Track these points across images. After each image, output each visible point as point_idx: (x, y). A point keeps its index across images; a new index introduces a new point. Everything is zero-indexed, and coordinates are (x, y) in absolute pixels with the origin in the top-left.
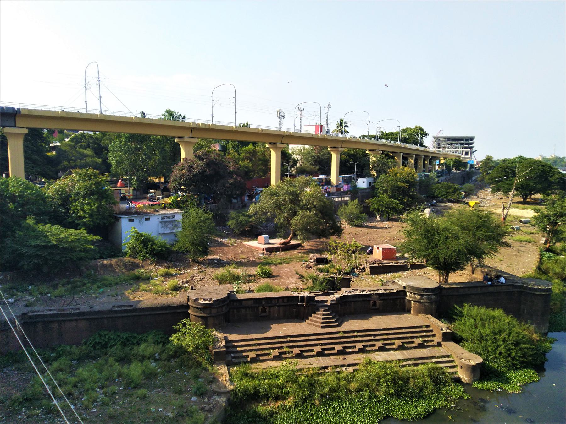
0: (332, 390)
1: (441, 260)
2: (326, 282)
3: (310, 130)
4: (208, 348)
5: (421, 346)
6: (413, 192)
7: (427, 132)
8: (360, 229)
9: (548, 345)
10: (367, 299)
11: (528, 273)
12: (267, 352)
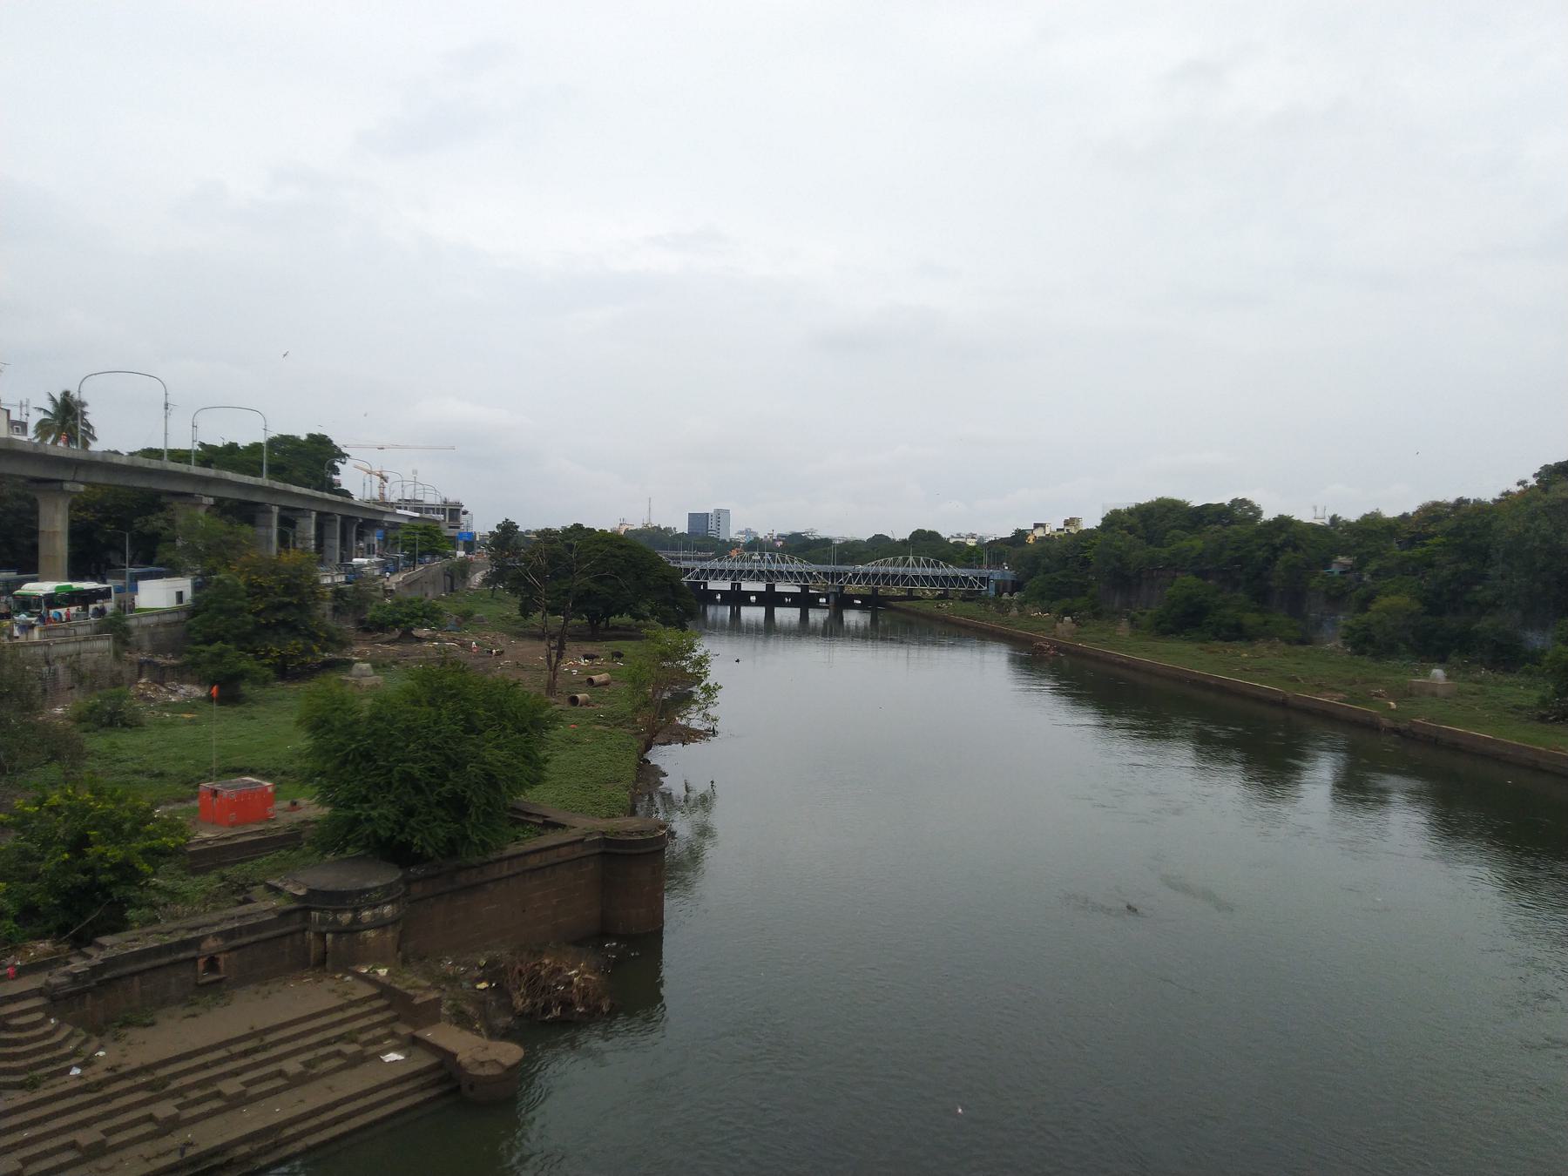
7: (344, 450)
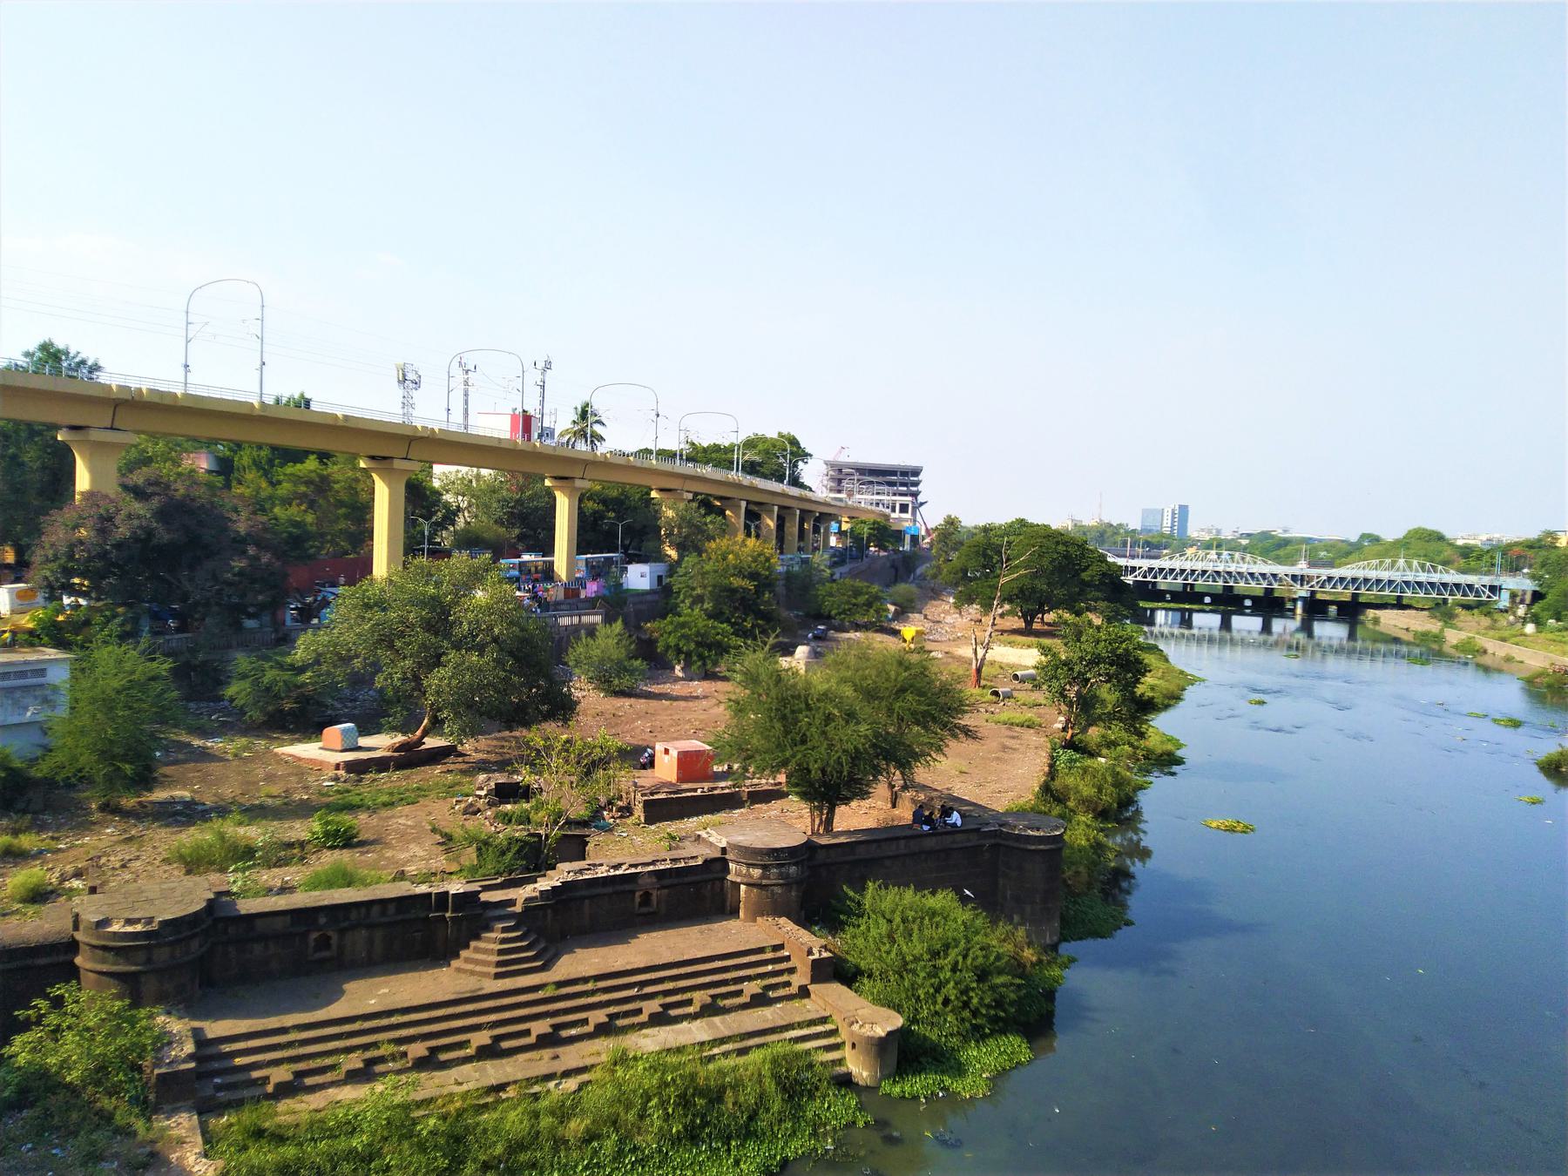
0: (516, 1147)
1: (815, 774)
2: (515, 849)
3: (495, 425)
4: (140, 1069)
5: (760, 1000)
6: (768, 603)
8: (626, 702)
9: (1056, 972)
10: (627, 887)
11: (1022, 801)
12: (328, 1061)
